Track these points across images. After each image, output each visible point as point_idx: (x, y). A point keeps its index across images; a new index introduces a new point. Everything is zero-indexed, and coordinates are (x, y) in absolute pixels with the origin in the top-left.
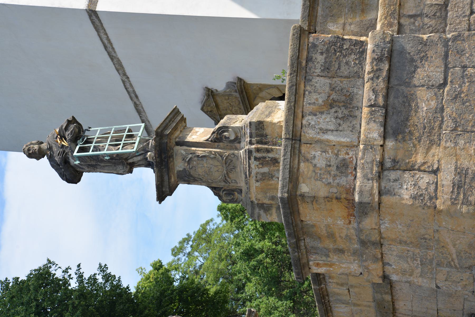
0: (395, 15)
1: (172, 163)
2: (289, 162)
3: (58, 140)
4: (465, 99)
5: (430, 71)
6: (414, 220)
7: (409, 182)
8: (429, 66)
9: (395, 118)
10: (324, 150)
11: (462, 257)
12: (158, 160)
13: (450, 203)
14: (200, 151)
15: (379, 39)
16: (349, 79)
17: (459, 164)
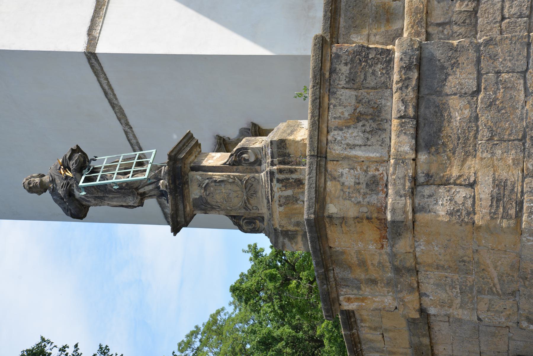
0: (422, 23)
1: (187, 190)
2: (314, 181)
3: (62, 171)
4: (500, 106)
5: (461, 78)
6: (452, 240)
7: (444, 197)
8: (461, 73)
9: (427, 130)
10: (352, 167)
11: (504, 281)
12: (172, 186)
13: (489, 218)
14: (217, 176)
15: (407, 46)
16: (376, 91)
17: (497, 176)
